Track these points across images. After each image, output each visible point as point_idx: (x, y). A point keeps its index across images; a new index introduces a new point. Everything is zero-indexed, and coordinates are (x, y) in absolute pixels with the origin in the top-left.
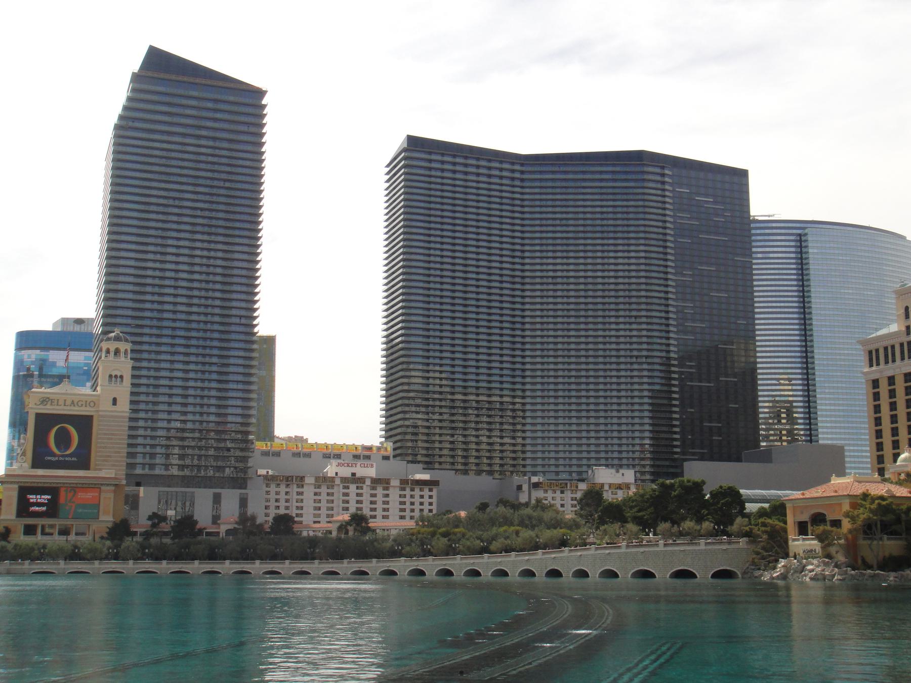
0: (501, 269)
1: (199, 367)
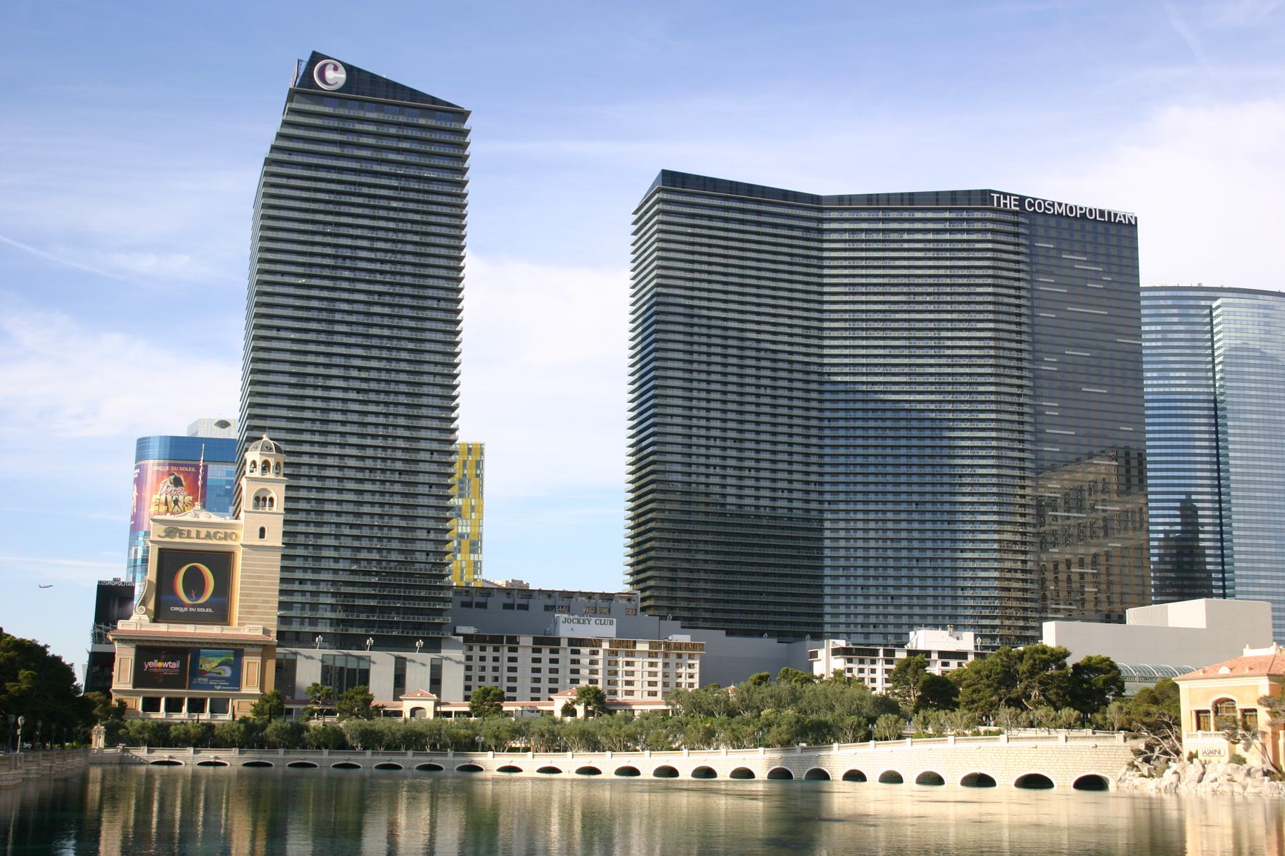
0: (791, 398)
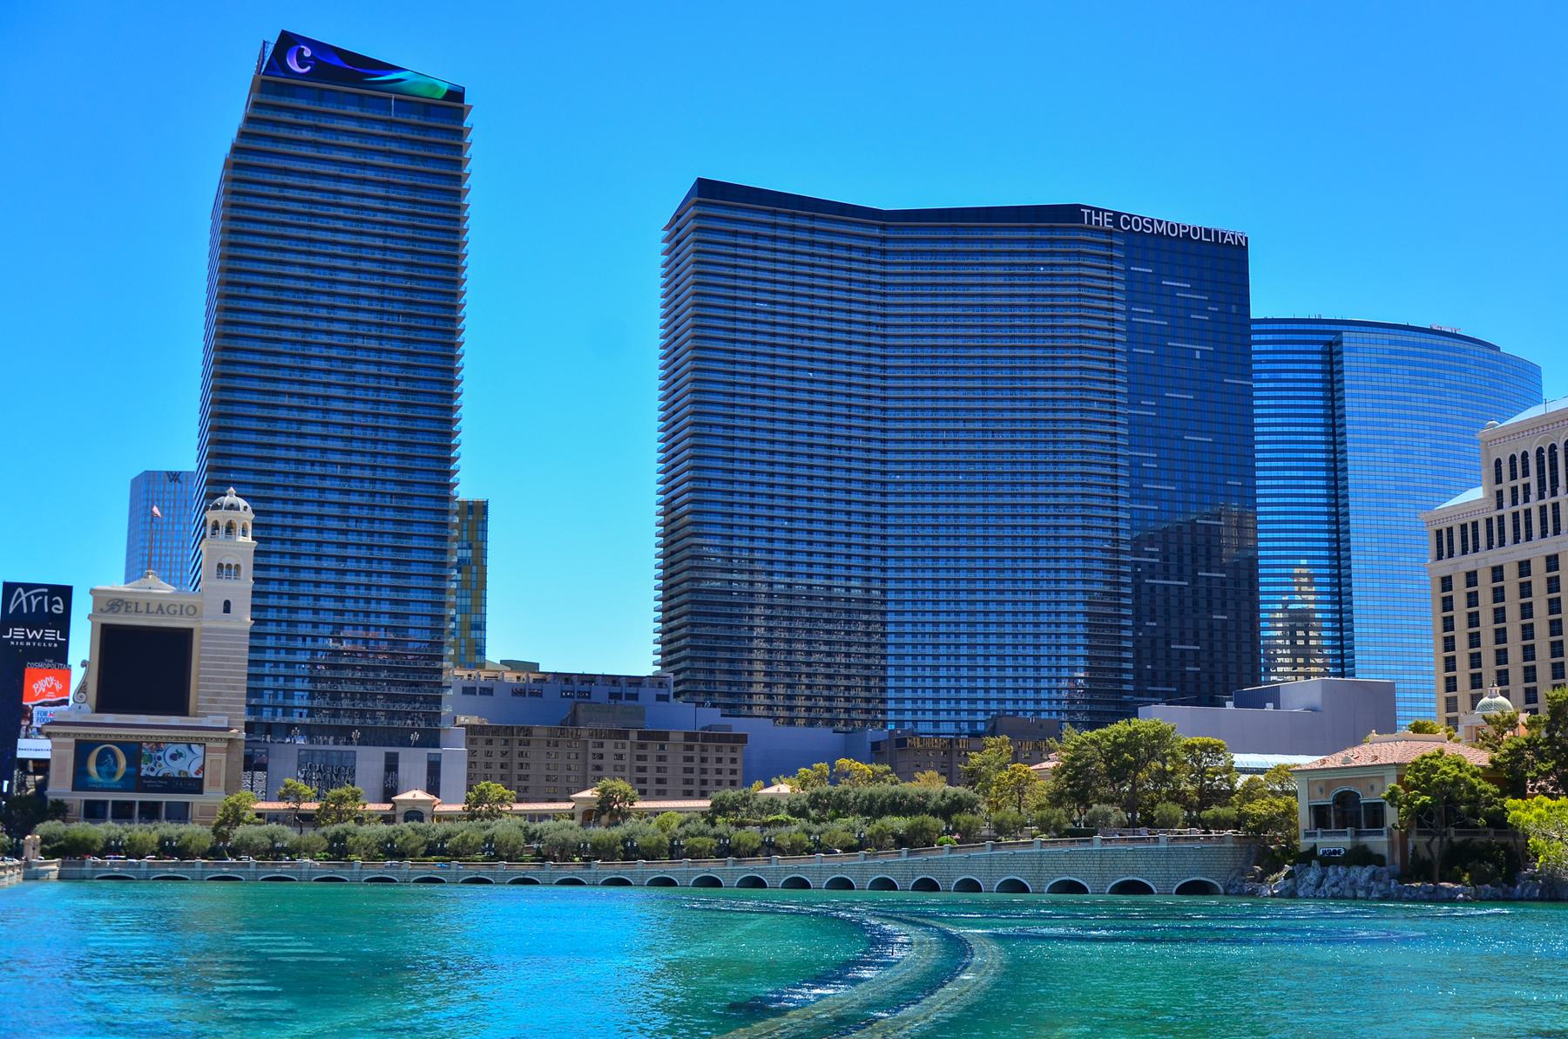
1: (364, 553)
